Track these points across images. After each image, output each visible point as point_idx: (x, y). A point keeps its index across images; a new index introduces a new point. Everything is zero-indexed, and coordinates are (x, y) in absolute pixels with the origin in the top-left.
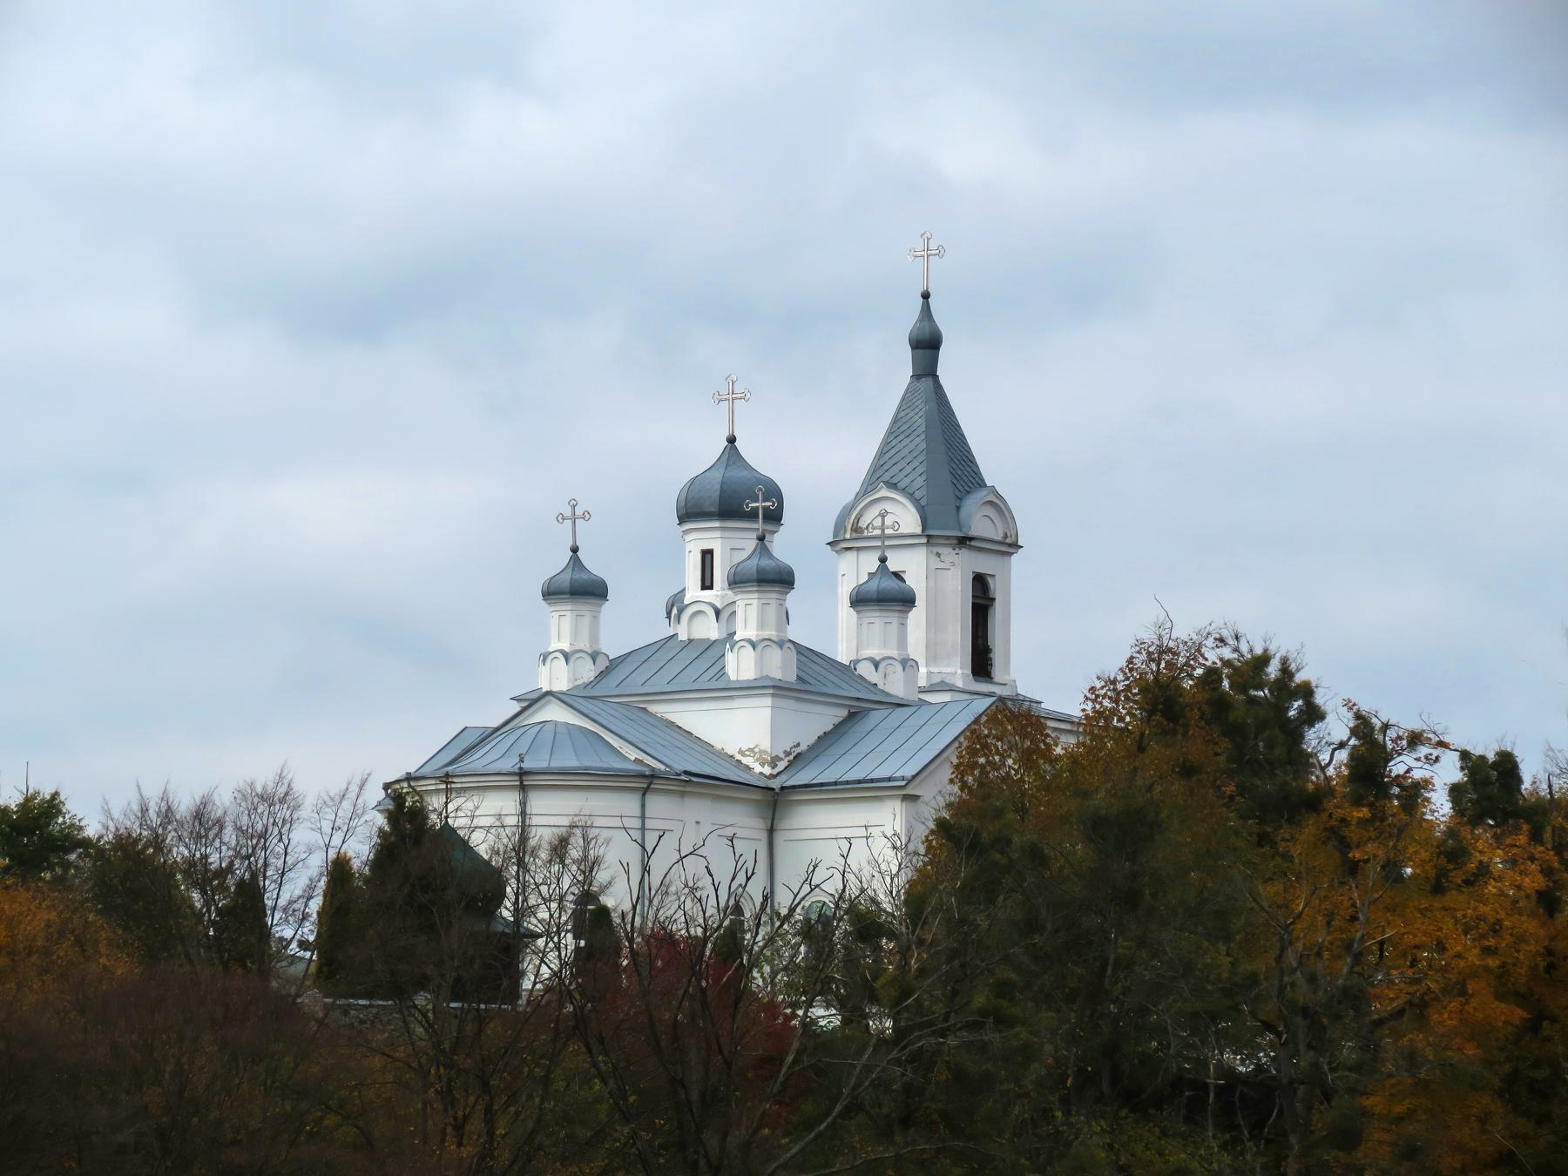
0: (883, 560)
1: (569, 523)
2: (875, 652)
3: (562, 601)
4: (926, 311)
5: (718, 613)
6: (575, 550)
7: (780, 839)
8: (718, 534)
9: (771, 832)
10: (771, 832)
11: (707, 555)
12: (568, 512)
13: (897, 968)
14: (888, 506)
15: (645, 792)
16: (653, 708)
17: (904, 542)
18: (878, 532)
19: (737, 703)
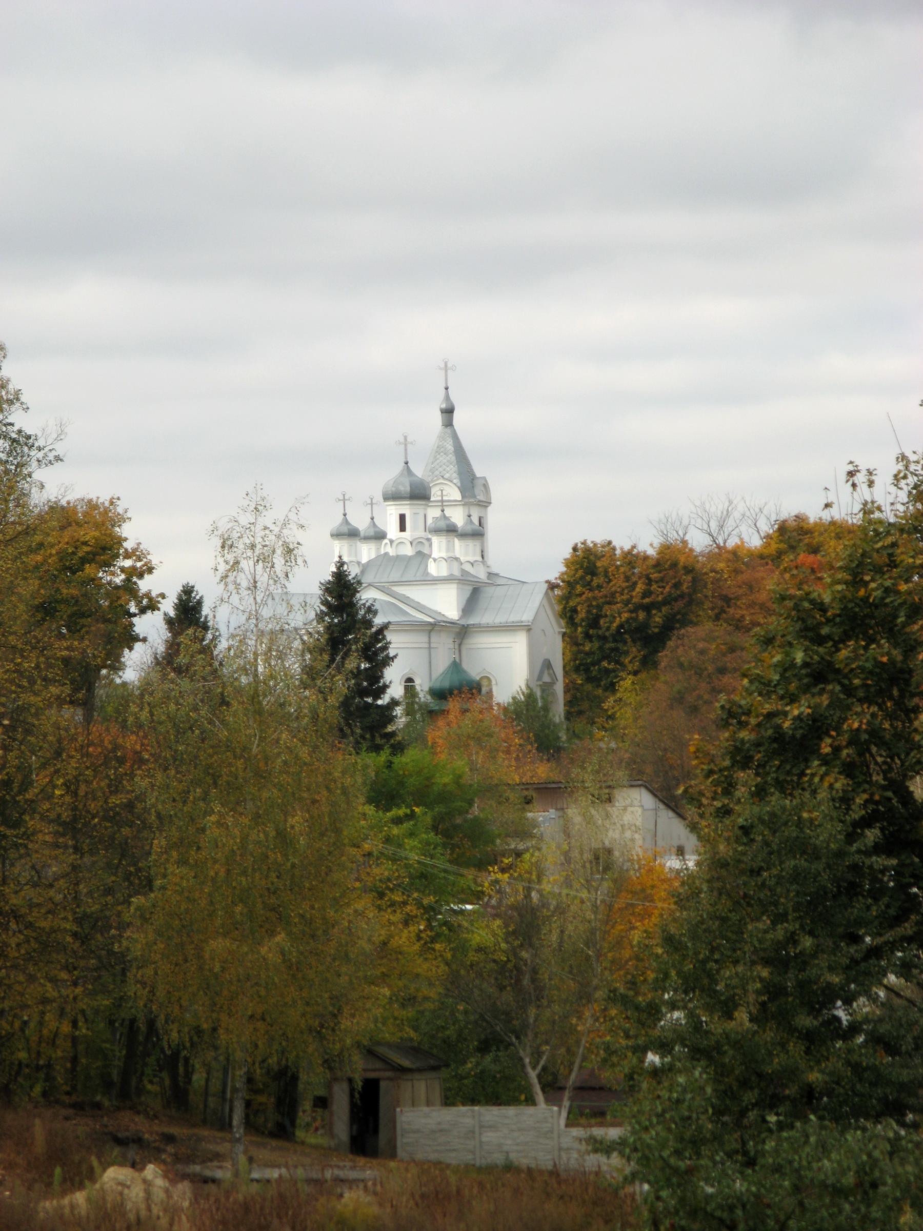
0: (443, 511)
1: (342, 503)
2: (471, 559)
3: (343, 539)
4: (447, 398)
5: (411, 543)
6: (372, 519)
7: (464, 648)
8: (393, 507)
9: (460, 645)
10: (460, 645)
11: (402, 518)
12: (342, 498)
13: (93, 716)
14: (445, 487)
15: (430, 631)
16: (395, 589)
17: (453, 503)
18: (440, 498)
19: (439, 586)
